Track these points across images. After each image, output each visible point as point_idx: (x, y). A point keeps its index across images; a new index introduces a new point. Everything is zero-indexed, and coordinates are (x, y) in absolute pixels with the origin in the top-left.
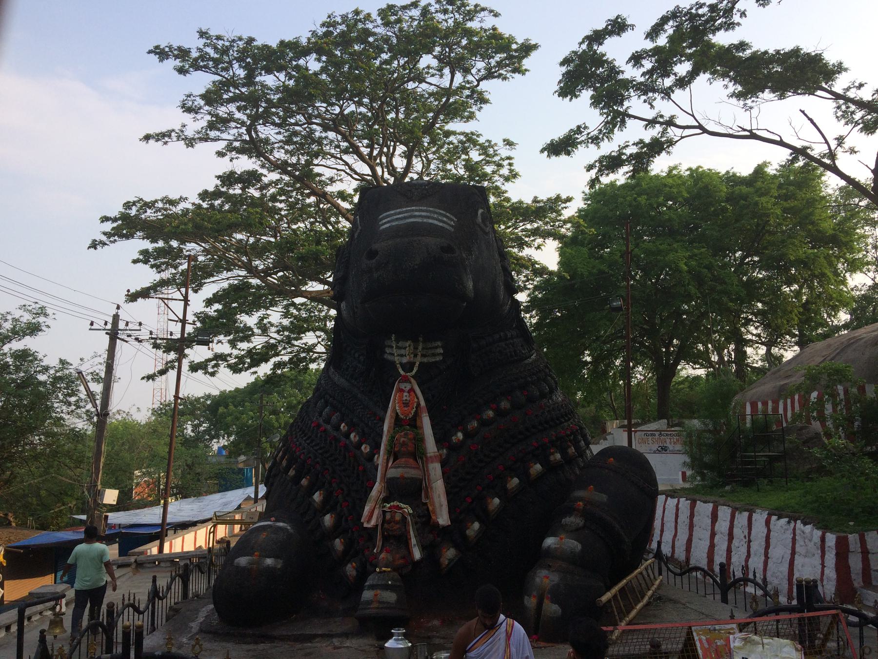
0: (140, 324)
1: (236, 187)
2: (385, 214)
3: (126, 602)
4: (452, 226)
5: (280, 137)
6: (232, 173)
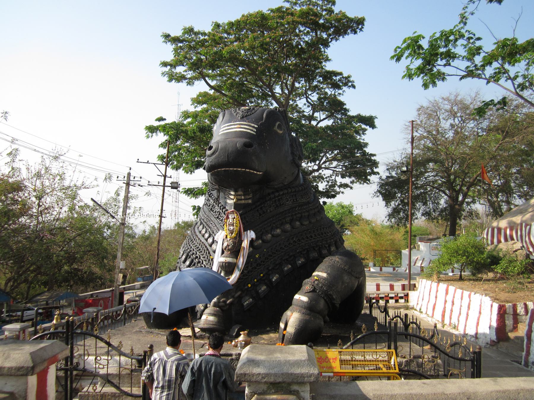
0: (141, 178)
3: (396, 315)
4: (254, 131)
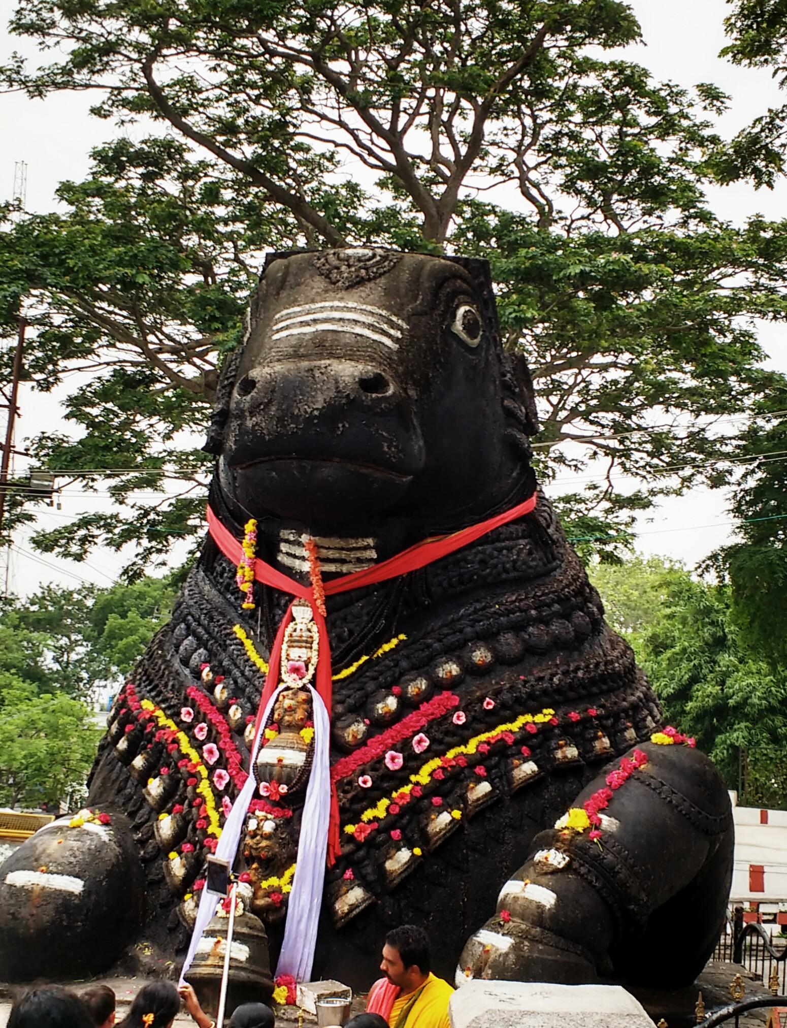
1: (131, 174)
2: (285, 312)
4: (396, 340)
5: (221, 77)
6: (123, 146)
